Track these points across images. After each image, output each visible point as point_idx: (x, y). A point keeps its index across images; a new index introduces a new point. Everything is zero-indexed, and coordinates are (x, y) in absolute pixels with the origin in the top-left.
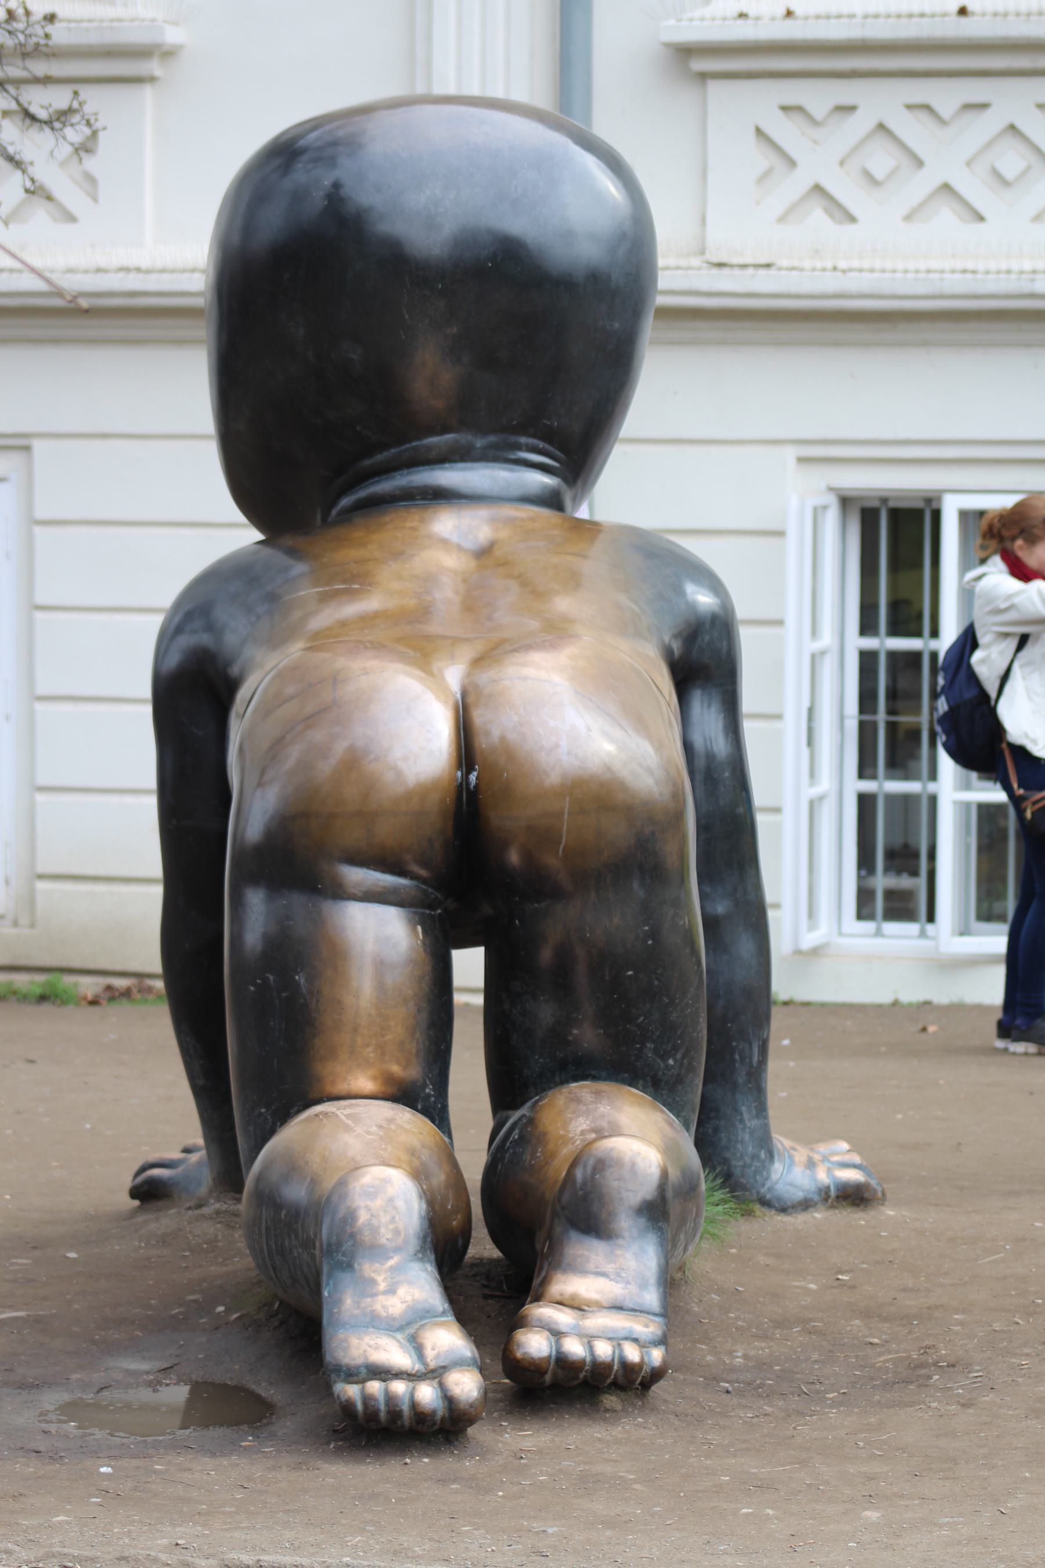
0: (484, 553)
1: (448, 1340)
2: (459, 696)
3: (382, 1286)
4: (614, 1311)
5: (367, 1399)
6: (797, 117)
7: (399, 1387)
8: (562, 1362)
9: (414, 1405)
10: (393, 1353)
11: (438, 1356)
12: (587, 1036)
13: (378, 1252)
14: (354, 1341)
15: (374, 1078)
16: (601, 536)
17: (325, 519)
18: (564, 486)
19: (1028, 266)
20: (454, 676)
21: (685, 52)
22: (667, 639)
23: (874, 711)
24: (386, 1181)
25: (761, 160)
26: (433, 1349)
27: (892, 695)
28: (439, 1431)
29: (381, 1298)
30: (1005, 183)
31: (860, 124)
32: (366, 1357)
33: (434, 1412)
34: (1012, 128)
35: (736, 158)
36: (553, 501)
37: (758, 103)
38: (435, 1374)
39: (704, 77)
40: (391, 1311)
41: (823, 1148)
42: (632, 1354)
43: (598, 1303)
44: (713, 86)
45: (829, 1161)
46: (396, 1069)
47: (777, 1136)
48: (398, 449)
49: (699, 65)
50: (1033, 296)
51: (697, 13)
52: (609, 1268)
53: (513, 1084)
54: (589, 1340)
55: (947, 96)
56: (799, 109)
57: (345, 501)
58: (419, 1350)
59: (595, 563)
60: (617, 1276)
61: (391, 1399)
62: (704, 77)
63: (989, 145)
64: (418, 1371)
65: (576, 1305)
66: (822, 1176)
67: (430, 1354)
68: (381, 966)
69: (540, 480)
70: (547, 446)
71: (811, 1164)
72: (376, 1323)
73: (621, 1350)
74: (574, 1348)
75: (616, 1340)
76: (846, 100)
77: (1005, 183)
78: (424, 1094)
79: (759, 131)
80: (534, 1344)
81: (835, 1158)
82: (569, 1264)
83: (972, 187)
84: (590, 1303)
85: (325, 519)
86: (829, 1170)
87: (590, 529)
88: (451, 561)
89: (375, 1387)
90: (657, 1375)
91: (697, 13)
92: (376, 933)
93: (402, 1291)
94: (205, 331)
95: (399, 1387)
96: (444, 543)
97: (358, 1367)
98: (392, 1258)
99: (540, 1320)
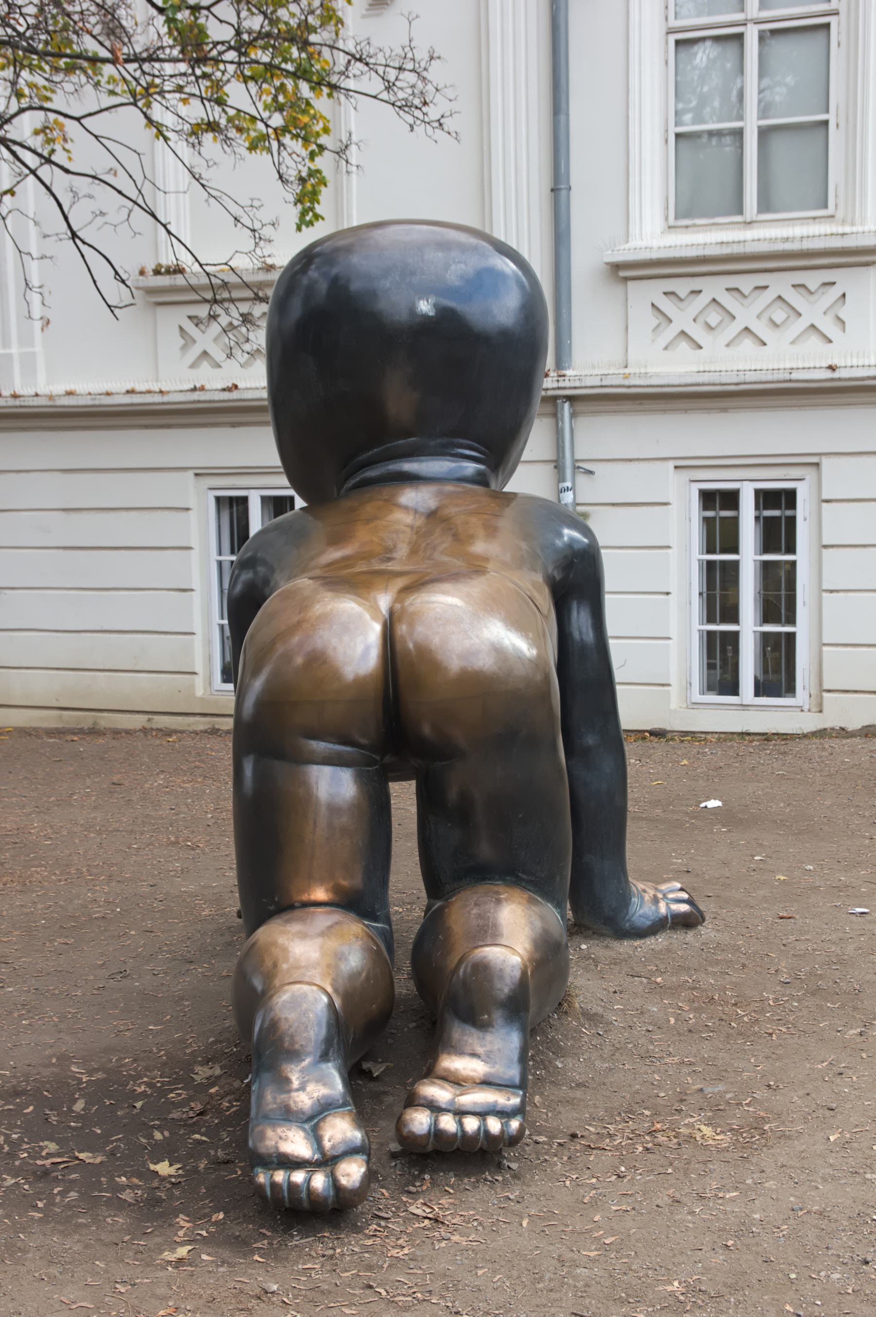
0: (432, 515)
1: (341, 1130)
2: (387, 616)
3: (296, 1084)
4: (485, 1086)
5: (274, 1185)
6: (672, 297)
7: (299, 1177)
8: (437, 1134)
9: (310, 1191)
10: (296, 1143)
11: (333, 1147)
12: (485, 850)
13: (294, 1055)
14: (270, 1133)
15: (327, 890)
16: (514, 504)
17: (339, 492)
18: (488, 471)
19: (788, 366)
20: (384, 601)
21: (616, 267)
22: (550, 571)
23: (715, 590)
24: (305, 996)
25: (653, 320)
26: (329, 1141)
27: (723, 581)
28: (332, 1213)
29: (294, 1094)
30: (776, 325)
31: (703, 300)
32: (277, 1148)
33: (326, 1199)
34: (780, 297)
35: (642, 319)
36: (481, 480)
37: (653, 291)
38: (327, 1161)
39: (626, 279)
40: (300, 1105)
41: (663, 887)
42: (494, 1125)
43: (469, 1084)
44: (630, 284)
45: (667, 898)
46: (345, 883)
47: (635, 882)
48: (379, 449)
49: (623, 274)
50: (790, 381)
51: (622, 247)
52: (480, 1050)
53: (440, 882)
54: (460, 1113)
55: (746, 283)
56: (673, 293)
57: (352, 482)
58: (317, 1139)
59: (506, 522)
60: (487, 1058)
61: (293, 1187)
62: (626, 279)
63: (768, 306)
64: (317, 1160)
65: (456, 1081)
66: (663, 909)
67: (327, 1145)
68: (334, 809)
69: (470, 468)
70: (476, 445)
71: (655, 901)
72: (288, 1115)
73: (485, 1125)
74: (448, 1123)
75: (482, 1115)
76: (697, 288)
77: (776, 325)
78: (362, 901)
79: (653, 305)
80: (420, 1121)
81: (671, 896)
82: (453, 1047)
83: (761, 329)
84: (466, 1079)
85: (339, 492)
86: (667, 904)
87: (511, 497)
88: (409, 519)
89: (280, 1176)
90: (514, 1140)
91: (622, 247)
92: (333, 785)
93: (310, 1087)
94: (269, 417)
95: (299, 1177)
96: (406, 508)
97: (270, 1155)
98: (304, 1060)
99: (425, 1098)
